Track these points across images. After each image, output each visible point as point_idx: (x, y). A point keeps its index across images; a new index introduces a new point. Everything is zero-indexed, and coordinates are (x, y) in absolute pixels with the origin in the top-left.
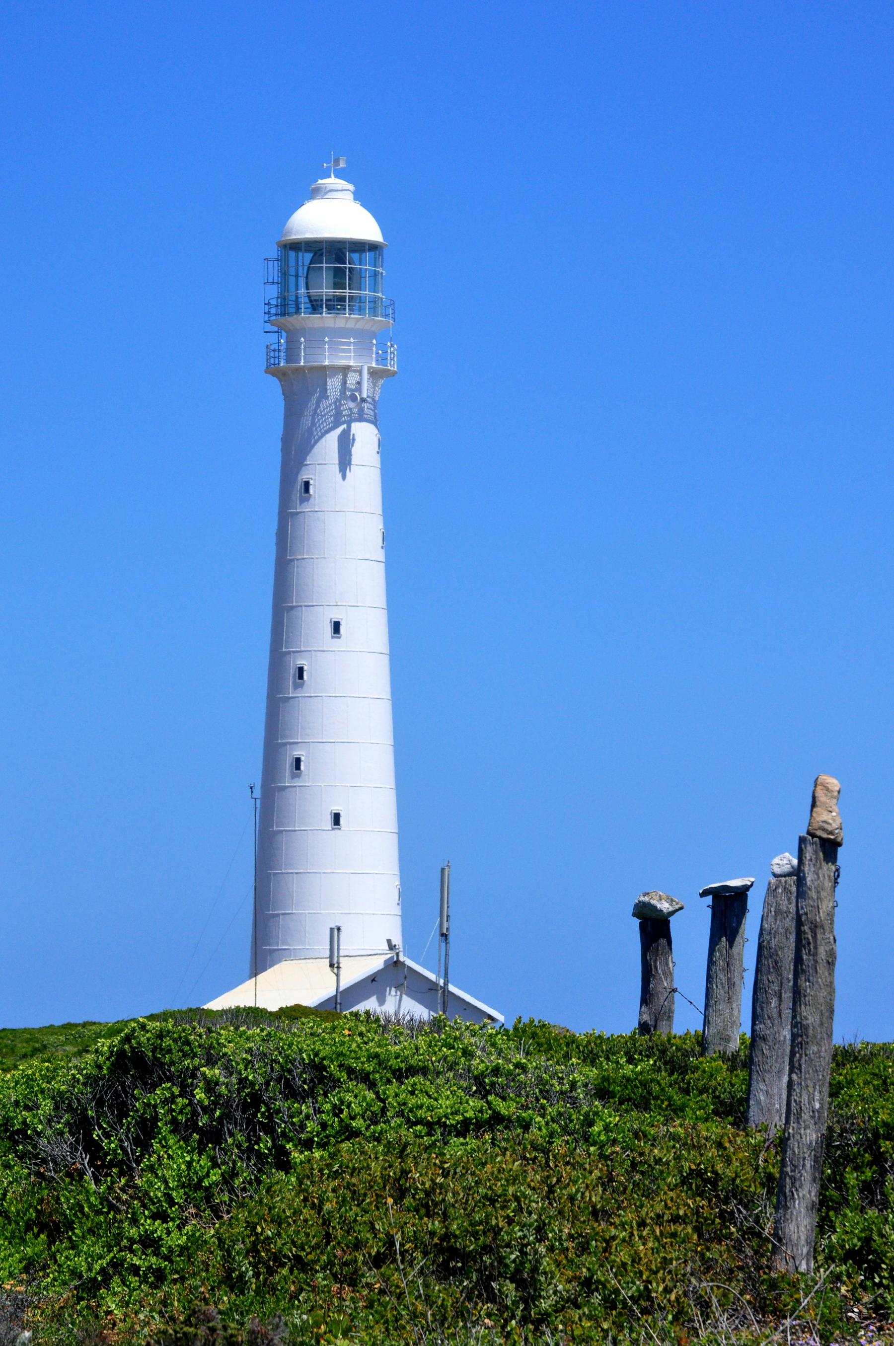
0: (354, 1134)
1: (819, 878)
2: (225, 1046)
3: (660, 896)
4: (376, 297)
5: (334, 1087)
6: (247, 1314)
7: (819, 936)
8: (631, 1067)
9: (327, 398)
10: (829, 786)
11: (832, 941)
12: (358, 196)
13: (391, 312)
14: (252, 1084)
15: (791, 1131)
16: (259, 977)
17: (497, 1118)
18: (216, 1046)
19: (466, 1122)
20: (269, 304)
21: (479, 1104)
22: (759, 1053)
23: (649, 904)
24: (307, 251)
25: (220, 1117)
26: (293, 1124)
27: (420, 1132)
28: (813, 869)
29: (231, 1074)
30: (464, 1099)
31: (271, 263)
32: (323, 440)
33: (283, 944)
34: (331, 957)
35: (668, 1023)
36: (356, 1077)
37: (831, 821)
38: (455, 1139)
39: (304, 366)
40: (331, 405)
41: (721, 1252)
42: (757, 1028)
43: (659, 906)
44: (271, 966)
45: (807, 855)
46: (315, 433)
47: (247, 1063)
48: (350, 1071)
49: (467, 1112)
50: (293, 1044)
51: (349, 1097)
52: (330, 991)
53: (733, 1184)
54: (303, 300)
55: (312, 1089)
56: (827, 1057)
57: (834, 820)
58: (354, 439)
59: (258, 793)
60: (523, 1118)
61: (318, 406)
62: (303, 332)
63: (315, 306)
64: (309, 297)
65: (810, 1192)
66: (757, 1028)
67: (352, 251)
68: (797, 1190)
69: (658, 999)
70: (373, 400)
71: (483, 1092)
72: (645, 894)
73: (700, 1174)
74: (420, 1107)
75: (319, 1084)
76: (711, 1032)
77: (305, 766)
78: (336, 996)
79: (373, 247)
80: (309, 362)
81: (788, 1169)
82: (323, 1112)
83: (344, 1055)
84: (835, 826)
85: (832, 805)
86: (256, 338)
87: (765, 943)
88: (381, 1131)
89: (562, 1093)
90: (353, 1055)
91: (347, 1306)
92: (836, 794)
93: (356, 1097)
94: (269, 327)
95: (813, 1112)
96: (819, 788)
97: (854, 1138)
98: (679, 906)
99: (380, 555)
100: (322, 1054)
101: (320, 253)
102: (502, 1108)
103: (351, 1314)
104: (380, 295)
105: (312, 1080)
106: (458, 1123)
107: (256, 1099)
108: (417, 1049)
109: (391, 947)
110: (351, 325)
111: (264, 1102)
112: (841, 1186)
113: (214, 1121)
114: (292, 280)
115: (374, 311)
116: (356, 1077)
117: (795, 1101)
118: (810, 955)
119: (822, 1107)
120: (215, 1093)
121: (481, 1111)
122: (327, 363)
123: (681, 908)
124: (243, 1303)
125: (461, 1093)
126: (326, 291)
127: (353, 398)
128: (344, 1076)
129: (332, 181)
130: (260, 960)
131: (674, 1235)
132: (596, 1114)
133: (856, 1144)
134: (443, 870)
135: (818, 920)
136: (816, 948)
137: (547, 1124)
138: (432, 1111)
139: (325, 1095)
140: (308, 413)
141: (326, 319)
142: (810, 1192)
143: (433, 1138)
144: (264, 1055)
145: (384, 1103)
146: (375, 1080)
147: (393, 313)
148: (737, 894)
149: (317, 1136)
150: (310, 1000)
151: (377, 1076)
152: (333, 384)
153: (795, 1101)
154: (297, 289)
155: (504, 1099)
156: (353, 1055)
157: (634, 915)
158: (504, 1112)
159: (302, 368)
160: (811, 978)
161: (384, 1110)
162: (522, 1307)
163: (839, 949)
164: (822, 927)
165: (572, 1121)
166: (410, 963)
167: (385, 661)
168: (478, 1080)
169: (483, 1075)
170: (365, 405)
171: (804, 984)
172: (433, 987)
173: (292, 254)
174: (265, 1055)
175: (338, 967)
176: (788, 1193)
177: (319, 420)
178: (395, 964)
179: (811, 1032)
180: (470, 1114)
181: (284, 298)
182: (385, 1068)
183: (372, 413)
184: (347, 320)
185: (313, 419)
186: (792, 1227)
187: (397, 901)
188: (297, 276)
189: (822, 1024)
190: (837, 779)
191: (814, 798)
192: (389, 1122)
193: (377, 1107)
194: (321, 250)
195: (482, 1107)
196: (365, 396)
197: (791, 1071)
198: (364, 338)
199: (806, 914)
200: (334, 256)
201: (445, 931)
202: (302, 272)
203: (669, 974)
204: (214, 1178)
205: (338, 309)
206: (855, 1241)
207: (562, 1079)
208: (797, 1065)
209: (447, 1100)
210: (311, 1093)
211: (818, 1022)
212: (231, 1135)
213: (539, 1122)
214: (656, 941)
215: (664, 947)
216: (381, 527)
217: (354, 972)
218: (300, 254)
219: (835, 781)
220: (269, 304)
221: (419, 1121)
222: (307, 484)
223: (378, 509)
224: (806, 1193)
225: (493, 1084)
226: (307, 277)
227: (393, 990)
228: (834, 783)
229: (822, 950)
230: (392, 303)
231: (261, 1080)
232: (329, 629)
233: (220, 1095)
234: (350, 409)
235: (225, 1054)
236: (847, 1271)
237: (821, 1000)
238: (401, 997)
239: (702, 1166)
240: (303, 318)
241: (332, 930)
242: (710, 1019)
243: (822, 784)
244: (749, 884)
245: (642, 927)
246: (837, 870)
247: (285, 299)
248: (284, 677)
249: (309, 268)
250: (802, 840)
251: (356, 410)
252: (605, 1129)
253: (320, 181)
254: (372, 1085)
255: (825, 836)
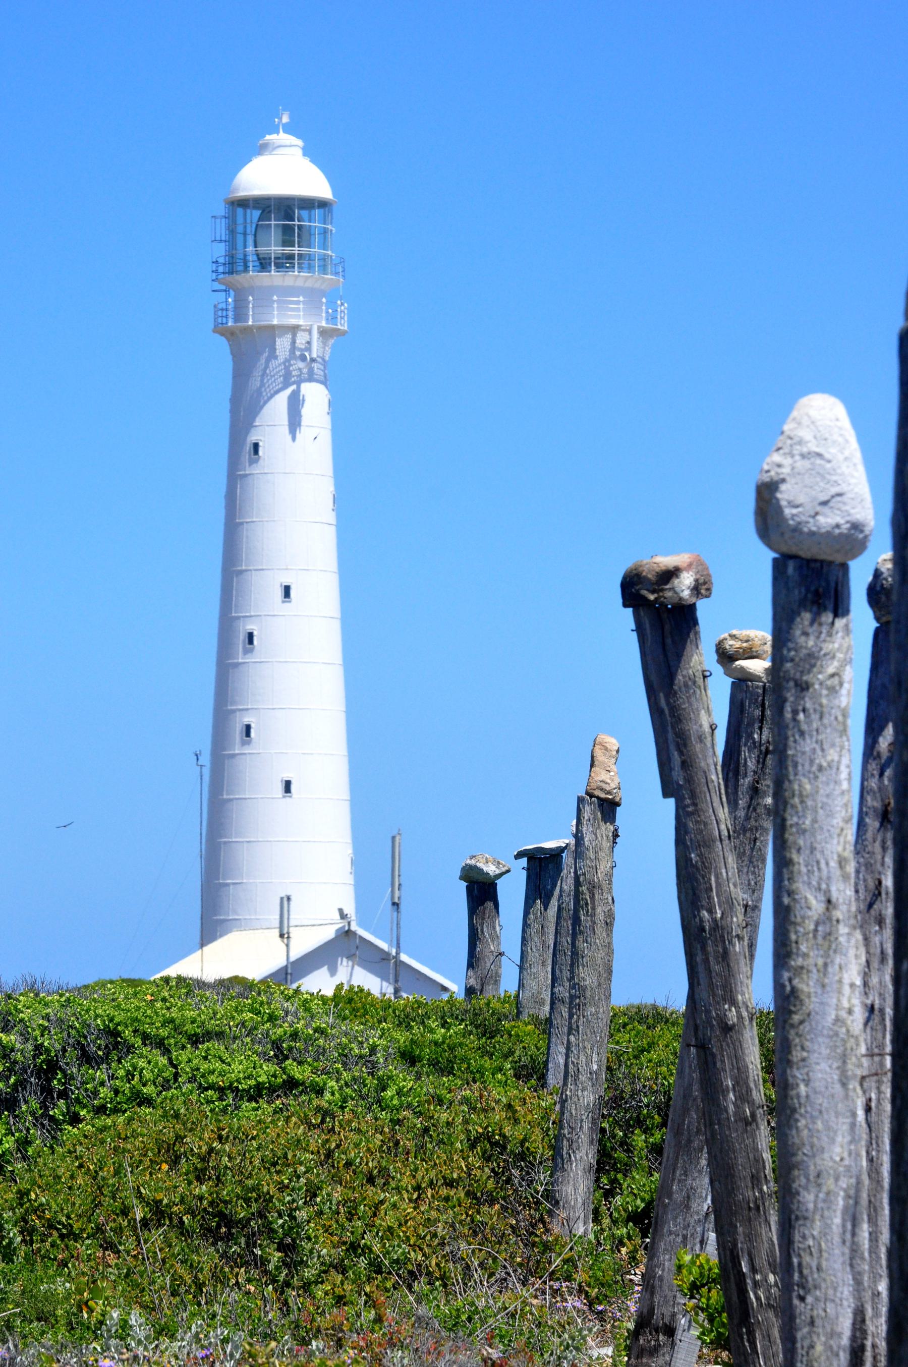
0: (147, 1101)
1: (597, 838)
2: (22, 1012)
3: (487, 859)
4: (325, 255)
5: (128, 1052)
6: (14, 1282)
7: (597, 897)
8: (443, 1031)
9: (276, 358)
10: (607, 745)
11: (610, 901)
12: (307, 152)
13: (341, 270)
14: (48, 1051)
15: (568, 1093)
16: (205, 949)
17: (291, 1084)
18: (14, 1012)
19: (259, 1087)
20: (217, 262)
21: (270, 1068)
22: (558, 1016)
23: (476, 866)
24: (255, 208)
25: (15, 1084)
26: (86, 1090)
27: (212, 1097)
28: (591, 829)
29: (27, 1040)
30: (258, 1065)
31: (218, 221)
32: (273, 400)
34: (281, 927)
35: (495, 987)
36: (151, 1043)
37: (609, 781)
38: (247, 1104)
39: (252, 326)
40: (280, 365)
41: (491, 1215)
42: (556, 990)
43: (485, 869)
44: (221, 936)
45: (585, 815)
46: (264, 394)
47: (44, 1030)
48: (145, 1037)
49: (259, 1076)
50: (90, 1009)
51: (142, 1063)
52: (281, 962)
53: (522, 1146)
54: (252, 258)
55: (107, 1055)
56: (605, 1019)
57: (613, 780)
58: (304, 400)
59: (206, 759)
60: (317, 1083)
61: (267, 367)
62: (251, 290)
63: (264, 264)
64: (258, 255)
65: (587, 1155)
66: (556, 990)
67: (301, 208)
68: (574, 1152)
69: (485, 963)
70: (323, 360)
71: (281, 1056)
72: (472, 857)
73: (488, 1137)
74: (212, 1072)
75: (114, 1049)
76: (525, 996)
78: (286, 966)
79: (323, 204)
80: (258, 321)
81: (566, 1131)
82: (117, 1078)
83: (139, 1021)
84: (613, 785)
85: (610, 764)
86: (204, 297)
87: (564, 905)
88: (172, 1097)
89: (361, 1057)
90: (148, 1020)
91: (110, 1273)
92: (614, 753)
93: (149, 1062)
94: (217, 286)
95: (591, 1073)
96: (597, 747)
97: (645, 1100)
98: (506, 868)
99: (331, 517)
100: (116, 1020)
101: (268, 210)
102: (297, 1072)
103: (115, 1281)
104: (329, 252)
105: (107, 1046)
106: (250, 1088)
107: (53, 1066)
108: (215, 1014)
109: (343, 916)
110: (300, 283)
111: (60, 1068)
112: (627, 1146)
113: (9, 1087)
114: (240, 238)
115: (324, 269)
116: (151, 1043)
117: (573, 1062)
118: (588, 916)
119: (599, 1069)
120: (10, 1059)
121: (275, 1076)
122: (275, 322)
123: (508, 871)
124: (11, 1271)
125: (255, 1058)
126: (275, 249)
127: (303, 358)
128: (138, 1042)
129: (283, 137)
130: (211, 927)
131: (447, 1199)
132: (390, 1078)
133: (647, 1106)
134: (393, 838)
135: (596, 880)
136: (594, 908)
137: (341, 1088)
138: (224, 1076)
139: (119, 1061)
140: (257, 373)
141: (274, 277)
142: (587, 1155)
143: (224, 1103)
144: (61, 1021)
145: (177, 1069)
146: (170, 1045)
147: (343, 271)
148: (552, 855)
149: (111, 1103)
150: (255, 972)
151: (172, 1041)
152: (283, 344)
153: (573, 1062)
154: (245, 247)
155: (300, 1063)
156: (148, 1020)
157: (461, 878)
158: (298, 1076)
159: (250, 328)
160: (589, 939)
161: (176, 1076)
162: (285, 1272)
163: (617, 909)
164: (600, 887)
165: (365, 1086)
166: (362, 932)
167: (336, 625)
168: (276, 1045)
169: (280, 1040)
170: (315, 365)
171: (581, 945)
172: (385, 957)
173: (240, 211)
174: (62, 1021)
175: (288, 937)
176: (565, 1156)
177: (268, 381)
178: (346, 934)
179: (588, 993)
180: (263, 1079)
181: (232, 257)
182: (181, 1033)
183: (322, 373)
184: (295, 277)
185: (262, 381)
186: (570, 1189)
187: (350, 870)
188: (245, 234)
189: (600, 985)
190: (616, 738)
191: (592, 757)
192: (181, 1088)
193: (169, 1073)
194: (269, 206)
195: (275, 1071)
196: (314, 355)
197: (569, 1034)
198: (313, 296)
199: (584, 874)
200: (283, 213)
201: (396, 900)
202: (251, 229)
203: (496, 938)
204: (7, 1146)
205: (287, 267)
206: (639, 1202)
207: (362, 1043)
208: (574, 1027)
209: (242, 1065)
210: (106, 1059)
211: (596, 983)
212: (26, 1102)
213: (332, 1087)
214: (482, 904)
215: (490, 911)
216: (332, 489)
217: (304, 942)
218: (249, 211)
219: (613, 741)
220: (217, 262)
221: (211, 1087)
222: (256, 446)
223: (330, 472)
224: (584, 1155)
225: (290, 1049)
226: (255, 235)
227: (345, 960)
228: (613, 743)
229: (600, 911)
230: (342, 261)
231: (58, 1047)
232: (280, 593)
233: (15, 1062)
234: (300, 369)
235: (21, 1020)
236: (628, 1233)
237: (599, 962)
238: (353, 968)
239: (490, 1129)
240: (251, 277)
241: (282, 899)
242: (525, 982)
243: (601, 744)
244: (564, 845)
245: (469, 890)
246: (616, 830)
247: (233, 257)
248: (233, 641)
249: (257, 225)
250: (580, 800)
251: (305, 371)
252: (398, 1094)
253: (268, 137)
254: (166, 1051)
255: (603, 795)
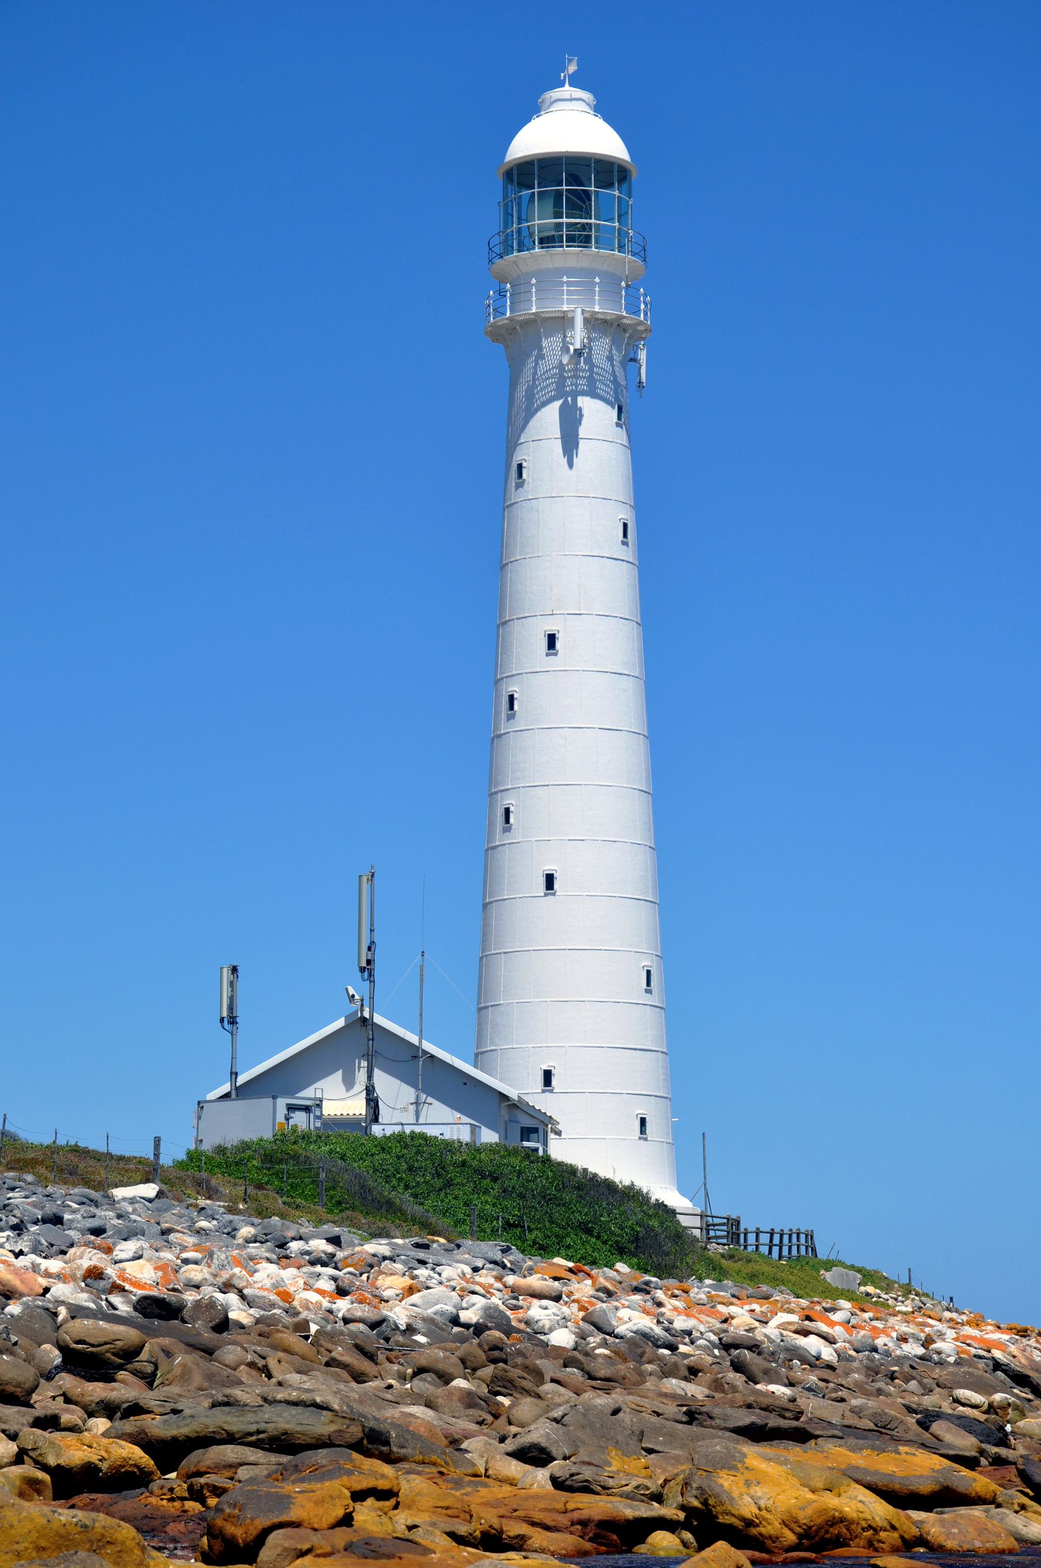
33: (491, 1045)
77: (515, 819)
222: (520, 467)
